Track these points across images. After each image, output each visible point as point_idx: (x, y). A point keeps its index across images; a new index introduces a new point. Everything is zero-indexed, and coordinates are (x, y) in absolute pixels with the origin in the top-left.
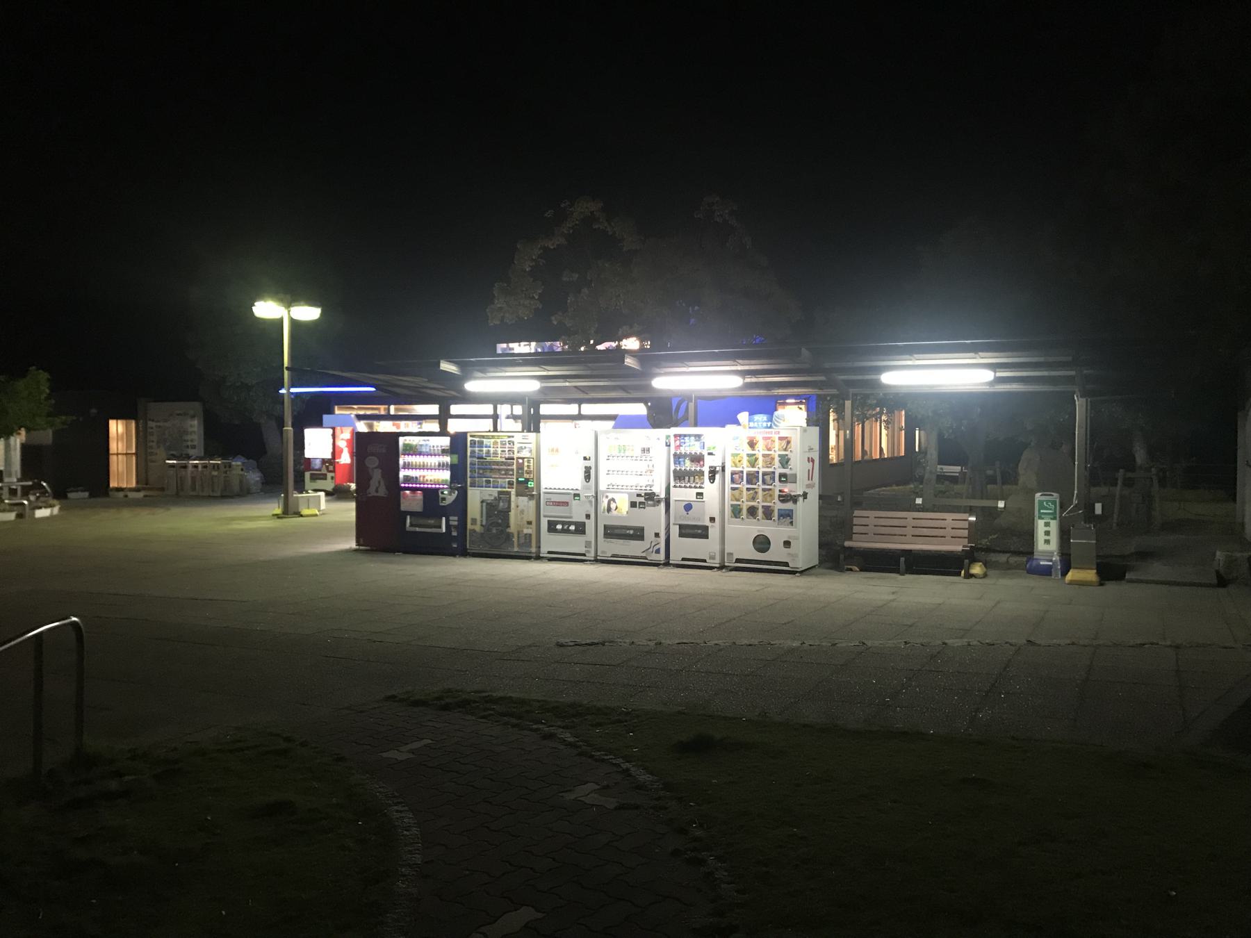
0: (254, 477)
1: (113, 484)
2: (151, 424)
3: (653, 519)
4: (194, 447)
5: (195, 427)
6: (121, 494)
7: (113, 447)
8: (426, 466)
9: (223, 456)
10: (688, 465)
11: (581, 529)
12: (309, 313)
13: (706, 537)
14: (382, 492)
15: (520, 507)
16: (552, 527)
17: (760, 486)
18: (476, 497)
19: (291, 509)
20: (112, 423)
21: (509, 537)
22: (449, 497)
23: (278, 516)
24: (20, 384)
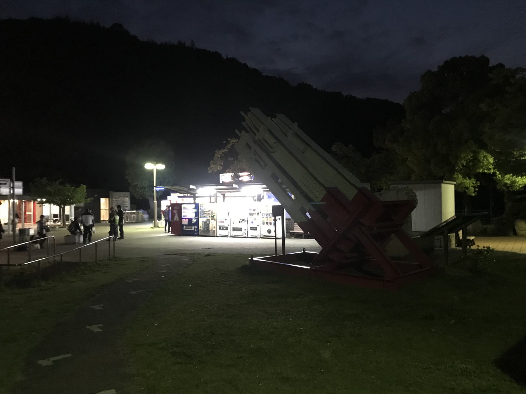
0: (146, 216)
1: (102, 219)
2: (113, 199)
3: (244, 226)
4: (127, 207)
5: (127, 200)
6: (104, 222)
7: (101, 208)
8: (188, 213)
9: (485, 173)
10: (252, 212)
11: (227, 228)
12: (161, 167)
13: (256, 230)
14: (178, 219)
15: (212, 224)
16: (220, 228)
17: (269, 217)
18: (201, 221)
19: (156, 226)
20: (101, 199)
21: (209, 231)
22: (194, 221)
23: (152, 228)
24: (79, 189)
